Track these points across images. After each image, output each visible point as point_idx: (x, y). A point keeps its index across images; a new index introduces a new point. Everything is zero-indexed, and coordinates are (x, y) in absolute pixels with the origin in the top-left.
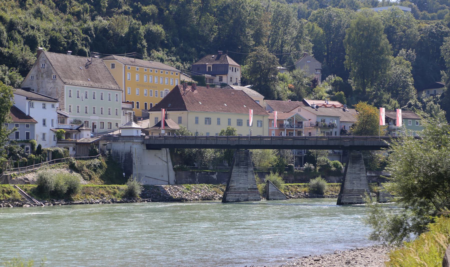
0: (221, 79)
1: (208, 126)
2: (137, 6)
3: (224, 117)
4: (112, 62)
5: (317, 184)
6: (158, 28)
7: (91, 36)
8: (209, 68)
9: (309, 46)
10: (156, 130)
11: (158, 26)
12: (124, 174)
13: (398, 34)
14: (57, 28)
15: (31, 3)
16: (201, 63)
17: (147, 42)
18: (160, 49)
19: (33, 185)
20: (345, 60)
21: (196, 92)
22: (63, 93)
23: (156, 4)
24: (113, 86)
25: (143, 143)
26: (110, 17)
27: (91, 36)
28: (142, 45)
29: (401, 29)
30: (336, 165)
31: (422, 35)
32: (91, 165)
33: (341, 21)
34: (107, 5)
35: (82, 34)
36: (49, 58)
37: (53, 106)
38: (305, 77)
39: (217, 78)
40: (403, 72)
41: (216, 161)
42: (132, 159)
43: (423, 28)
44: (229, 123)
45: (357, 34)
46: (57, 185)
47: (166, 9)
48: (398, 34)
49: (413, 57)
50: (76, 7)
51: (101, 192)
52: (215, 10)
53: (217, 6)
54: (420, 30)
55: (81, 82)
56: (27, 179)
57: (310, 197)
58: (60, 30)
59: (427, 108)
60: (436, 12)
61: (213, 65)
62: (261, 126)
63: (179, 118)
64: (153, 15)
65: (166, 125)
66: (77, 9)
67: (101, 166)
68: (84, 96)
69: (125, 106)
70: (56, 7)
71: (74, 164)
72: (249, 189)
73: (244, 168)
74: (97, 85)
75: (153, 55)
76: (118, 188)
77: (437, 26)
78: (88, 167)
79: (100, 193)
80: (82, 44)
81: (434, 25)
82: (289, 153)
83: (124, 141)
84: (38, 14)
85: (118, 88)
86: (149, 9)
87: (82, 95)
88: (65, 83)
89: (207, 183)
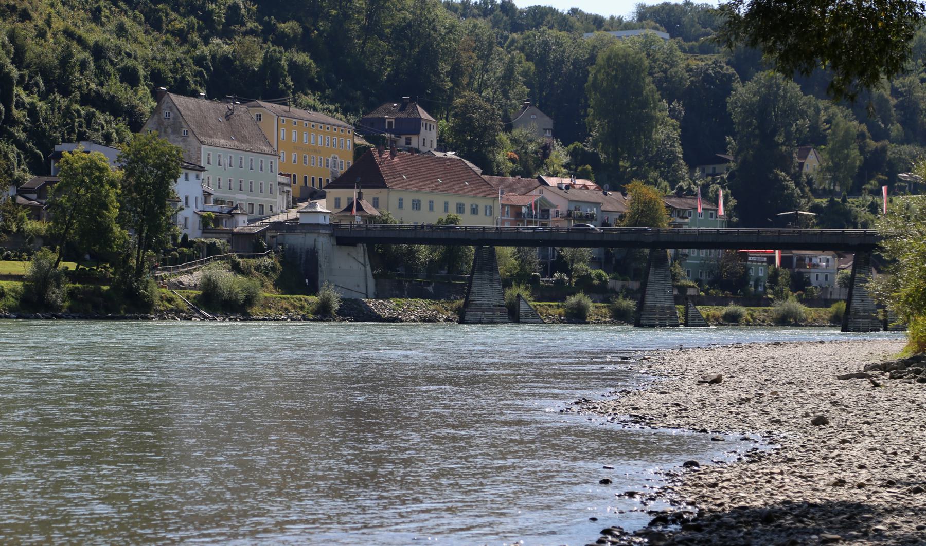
0: (408, 142)
1: (416, 212)
2: (269, 22)
3: (439, 200)
4: (258, 111)
5: (578, 303)
6: (303, 58)
7: (207, 69)
8: (390, 123)
9: (523, 92)
10: (347, 216)
11: (303, 55)
12: (307, 280)
13: (656, 75)
14: (159, 56)
15: (108, 15)
16: (376, 116)
17: (292, 80)
18: (309, 92)
19: (196, 292)
20: (588, 115)
21: (396, 159)
22: (200, 158)
23: (299, 20)
24: (266, 149)
25: (332, 235)
26: (230, 39)
27: (207, 69)
28: (285, 84)
29: (660, 67)
30: (599, 277)
31: (692, 78)
32: (260, 265)
33: (564, 52)
34: (224, 20)
35: (193, 66)
36: (176, 104)
37: (198, 177)
38: (531, 141)
39: (402, 140)
40: (668, 137)
41: (432, 266)
42: (317, 260)
43: (695, 67)
44: (446, 209)
45: (608, 74)
46: (230, 291)
47: (313, 28)
48: (656, 75)
49: (680, 113)
50: (177, 22)
51: (284, 306)
52: (388, 30)
53: (392, 24)
54: (689, 69)
55: (223, 141)
56: (182, 283)
57: (566, 323)
58: (164, 59)
59: (711, 195)
60: (696, 39)
61: (396, 119)
62: (491, 214)
63: (336, 199)
64: (295, 35)
65: (360, 208)
66: (178, 26)
67: (273, 269)
68: (227, 163)
69: (283, 179)
70: (145, 21)
71: (239, 262)
72: (494, 306)
73: (489, 274)
74: (244, 146)
75: (299, 101)
76: (306, 300)
77: (716, 65)
78: (258, 268)
79: (282, 307)
80: (195, 82)
81: (710, 62)
82: (534, 254)
83: (304, 231)
84: (121, 30)
85: (273, 153)
86: (288, 27)
87: (225, 161)
88: (202, 143)
89: (423, 297)
